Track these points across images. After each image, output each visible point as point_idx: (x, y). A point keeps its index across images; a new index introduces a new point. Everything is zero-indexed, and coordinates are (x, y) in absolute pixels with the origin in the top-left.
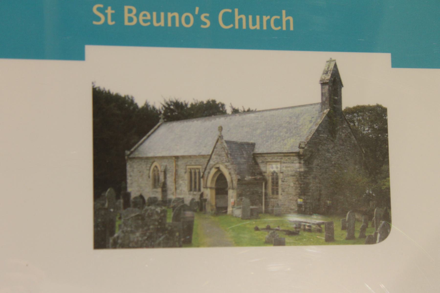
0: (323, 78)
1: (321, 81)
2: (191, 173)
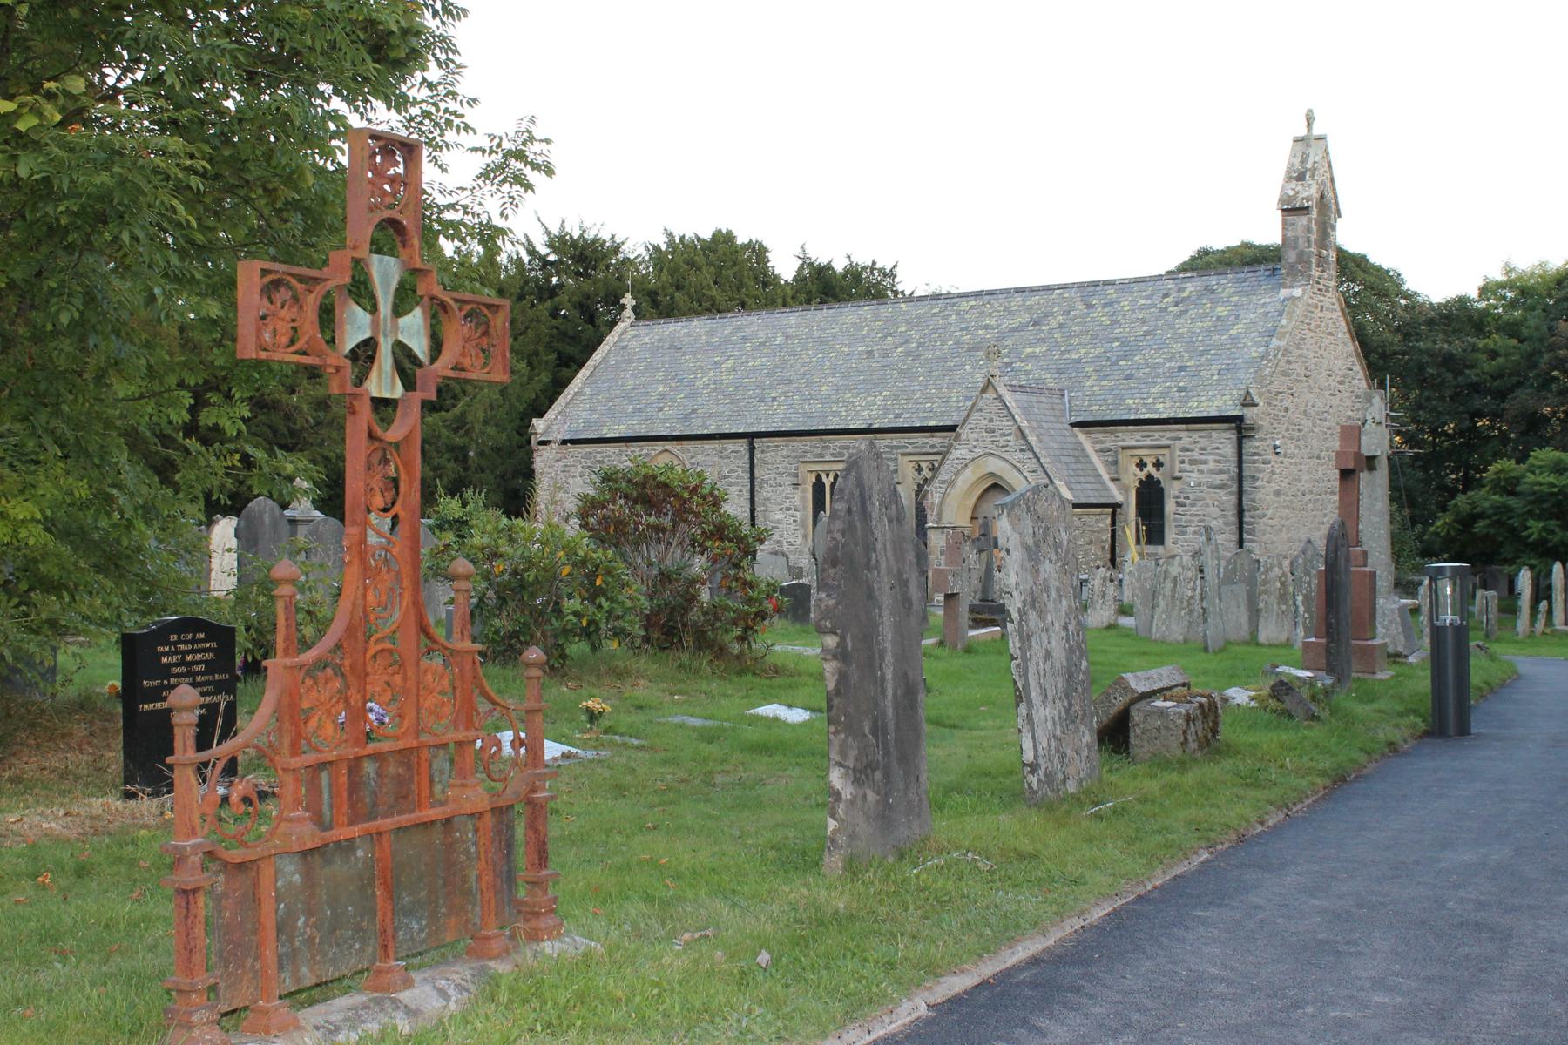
0: (1291, 193)
1: (1281, 201)
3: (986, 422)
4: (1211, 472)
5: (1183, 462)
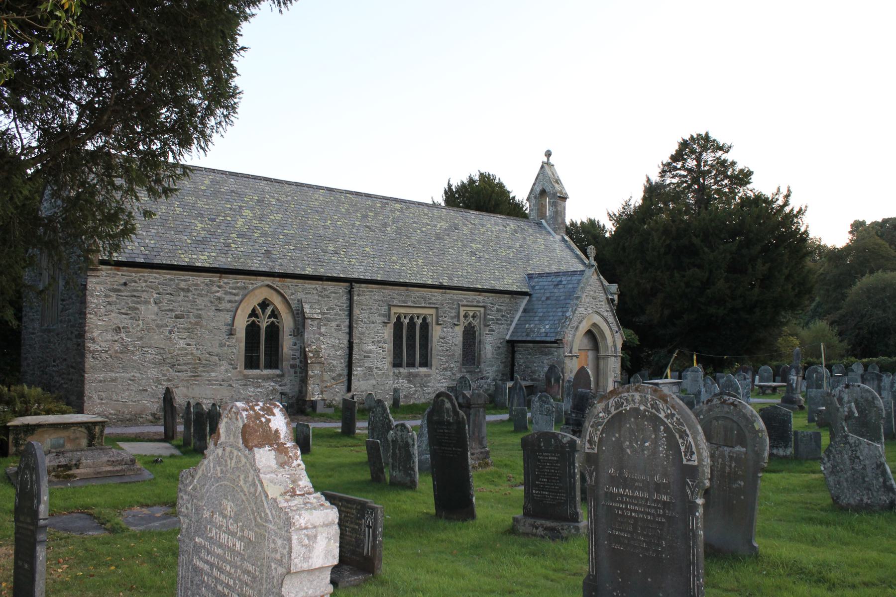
2: (398, 325)
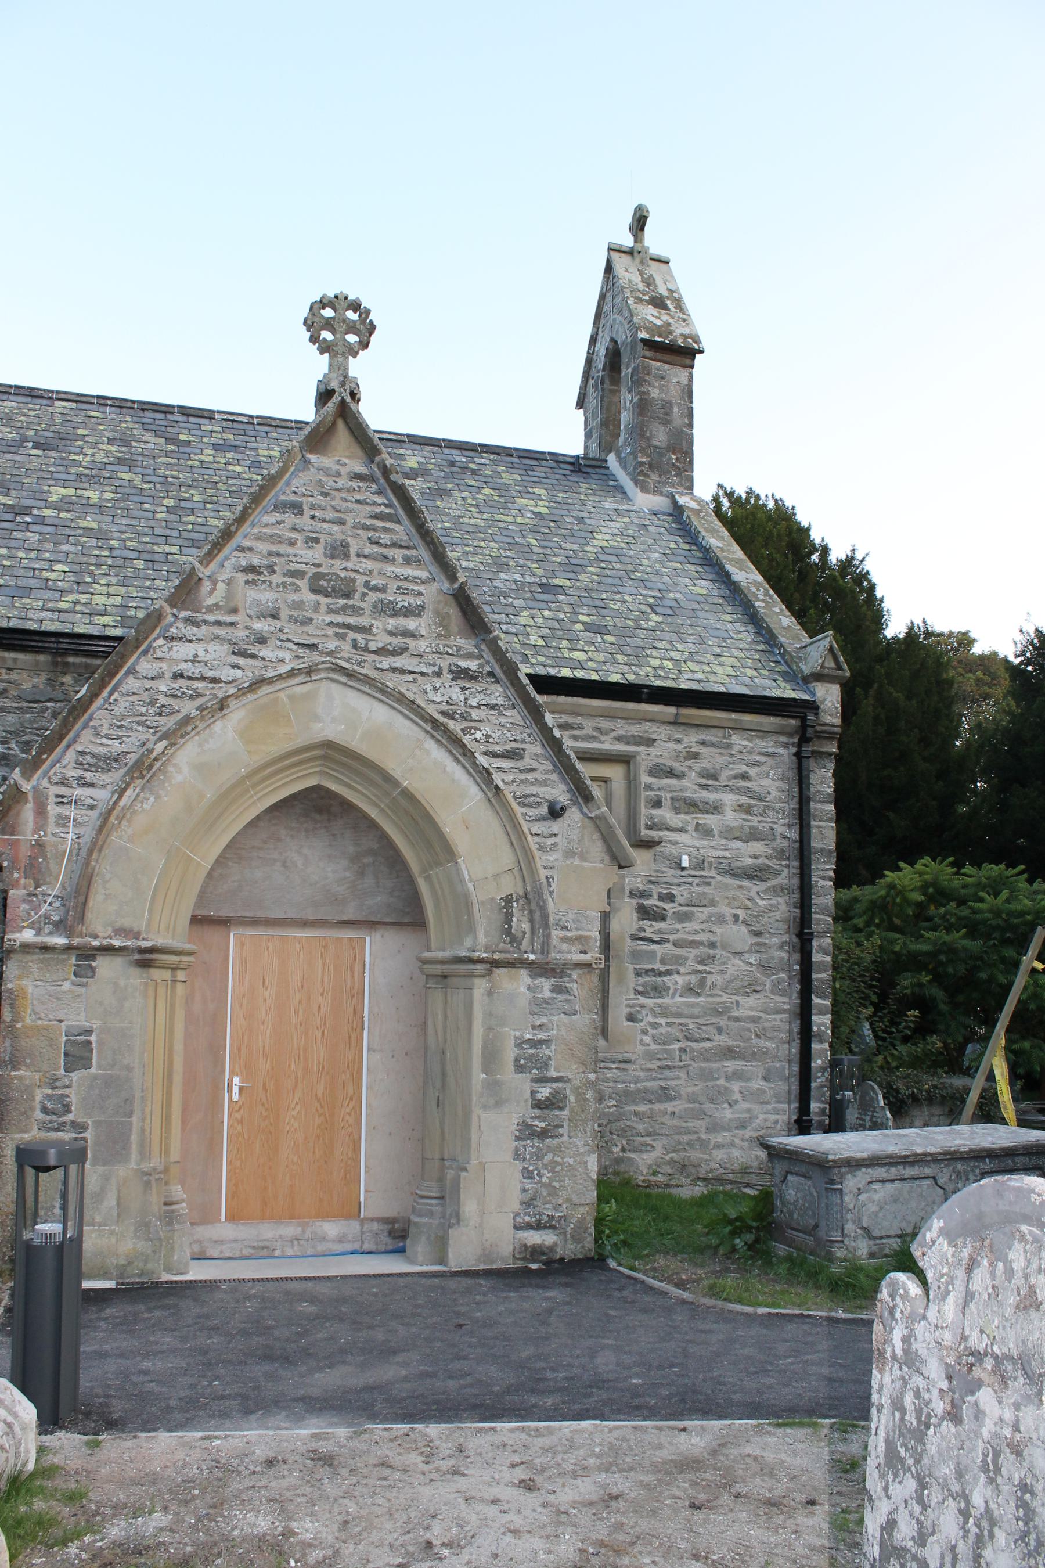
3: (316, 554)
4: (729, 834)
5: (657, 804)
